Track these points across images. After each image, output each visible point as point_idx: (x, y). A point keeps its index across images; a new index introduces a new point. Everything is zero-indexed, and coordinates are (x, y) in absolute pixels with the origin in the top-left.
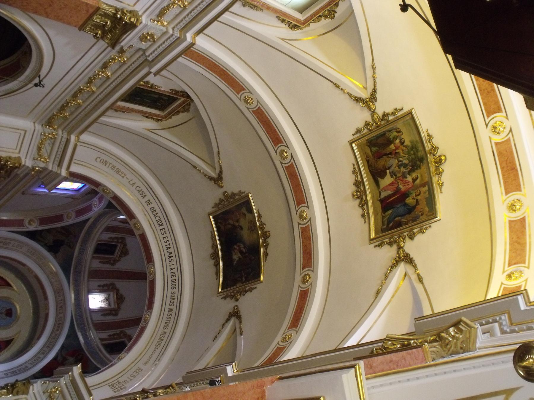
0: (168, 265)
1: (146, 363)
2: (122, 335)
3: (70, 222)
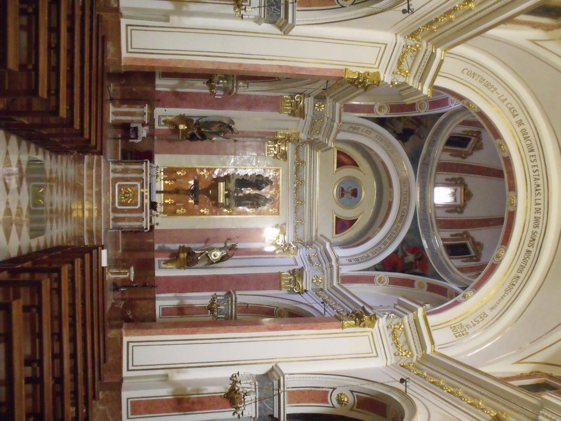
0: (534, 198)
1: (492, 308)
2: (465, 236)
3: (423, 113)
